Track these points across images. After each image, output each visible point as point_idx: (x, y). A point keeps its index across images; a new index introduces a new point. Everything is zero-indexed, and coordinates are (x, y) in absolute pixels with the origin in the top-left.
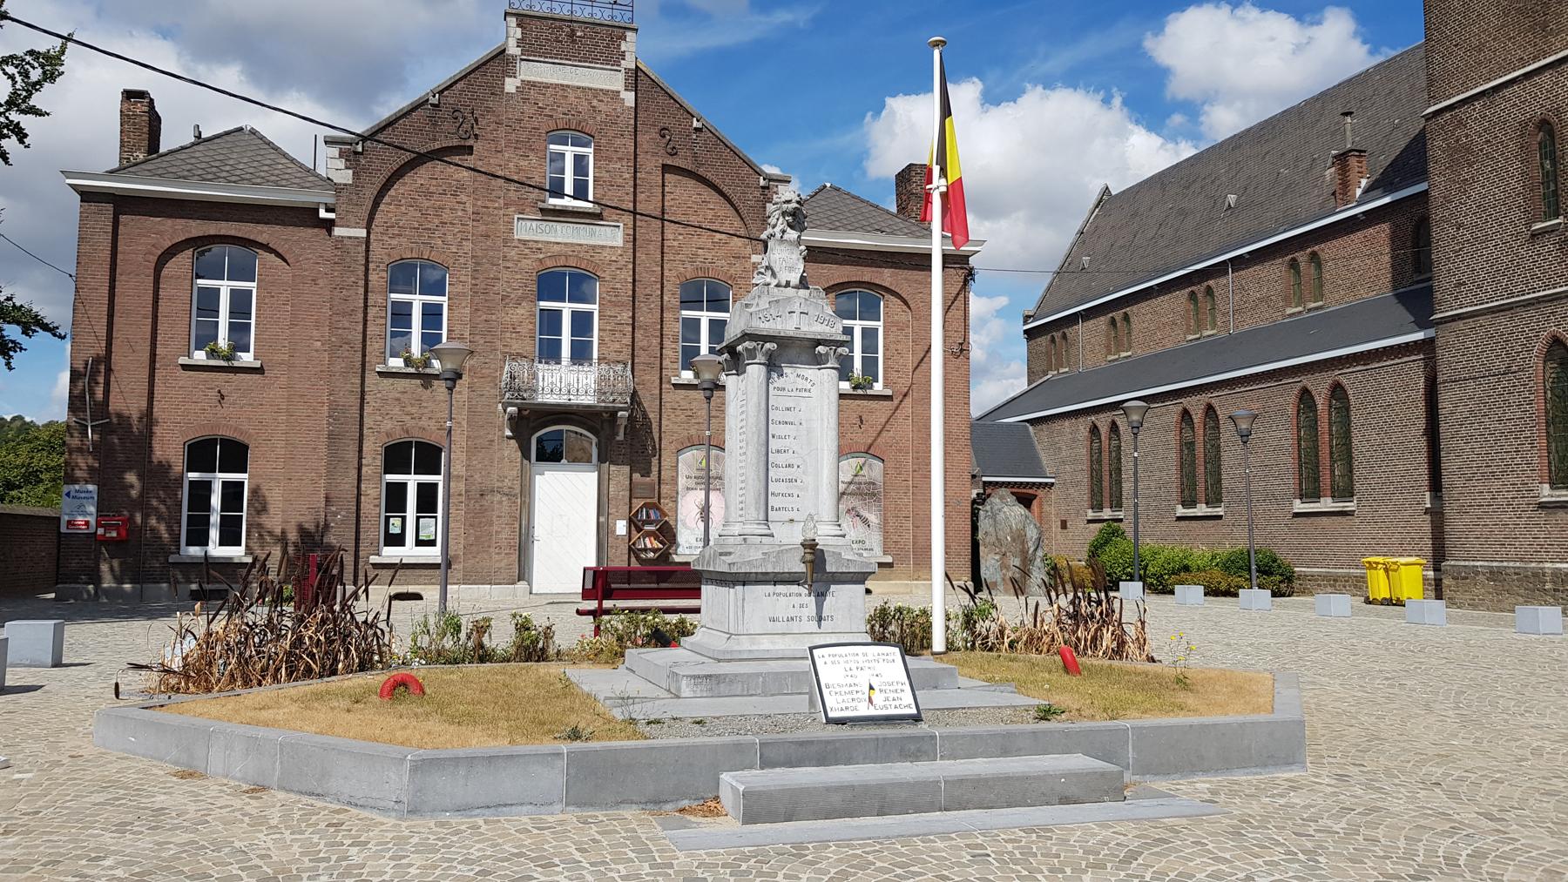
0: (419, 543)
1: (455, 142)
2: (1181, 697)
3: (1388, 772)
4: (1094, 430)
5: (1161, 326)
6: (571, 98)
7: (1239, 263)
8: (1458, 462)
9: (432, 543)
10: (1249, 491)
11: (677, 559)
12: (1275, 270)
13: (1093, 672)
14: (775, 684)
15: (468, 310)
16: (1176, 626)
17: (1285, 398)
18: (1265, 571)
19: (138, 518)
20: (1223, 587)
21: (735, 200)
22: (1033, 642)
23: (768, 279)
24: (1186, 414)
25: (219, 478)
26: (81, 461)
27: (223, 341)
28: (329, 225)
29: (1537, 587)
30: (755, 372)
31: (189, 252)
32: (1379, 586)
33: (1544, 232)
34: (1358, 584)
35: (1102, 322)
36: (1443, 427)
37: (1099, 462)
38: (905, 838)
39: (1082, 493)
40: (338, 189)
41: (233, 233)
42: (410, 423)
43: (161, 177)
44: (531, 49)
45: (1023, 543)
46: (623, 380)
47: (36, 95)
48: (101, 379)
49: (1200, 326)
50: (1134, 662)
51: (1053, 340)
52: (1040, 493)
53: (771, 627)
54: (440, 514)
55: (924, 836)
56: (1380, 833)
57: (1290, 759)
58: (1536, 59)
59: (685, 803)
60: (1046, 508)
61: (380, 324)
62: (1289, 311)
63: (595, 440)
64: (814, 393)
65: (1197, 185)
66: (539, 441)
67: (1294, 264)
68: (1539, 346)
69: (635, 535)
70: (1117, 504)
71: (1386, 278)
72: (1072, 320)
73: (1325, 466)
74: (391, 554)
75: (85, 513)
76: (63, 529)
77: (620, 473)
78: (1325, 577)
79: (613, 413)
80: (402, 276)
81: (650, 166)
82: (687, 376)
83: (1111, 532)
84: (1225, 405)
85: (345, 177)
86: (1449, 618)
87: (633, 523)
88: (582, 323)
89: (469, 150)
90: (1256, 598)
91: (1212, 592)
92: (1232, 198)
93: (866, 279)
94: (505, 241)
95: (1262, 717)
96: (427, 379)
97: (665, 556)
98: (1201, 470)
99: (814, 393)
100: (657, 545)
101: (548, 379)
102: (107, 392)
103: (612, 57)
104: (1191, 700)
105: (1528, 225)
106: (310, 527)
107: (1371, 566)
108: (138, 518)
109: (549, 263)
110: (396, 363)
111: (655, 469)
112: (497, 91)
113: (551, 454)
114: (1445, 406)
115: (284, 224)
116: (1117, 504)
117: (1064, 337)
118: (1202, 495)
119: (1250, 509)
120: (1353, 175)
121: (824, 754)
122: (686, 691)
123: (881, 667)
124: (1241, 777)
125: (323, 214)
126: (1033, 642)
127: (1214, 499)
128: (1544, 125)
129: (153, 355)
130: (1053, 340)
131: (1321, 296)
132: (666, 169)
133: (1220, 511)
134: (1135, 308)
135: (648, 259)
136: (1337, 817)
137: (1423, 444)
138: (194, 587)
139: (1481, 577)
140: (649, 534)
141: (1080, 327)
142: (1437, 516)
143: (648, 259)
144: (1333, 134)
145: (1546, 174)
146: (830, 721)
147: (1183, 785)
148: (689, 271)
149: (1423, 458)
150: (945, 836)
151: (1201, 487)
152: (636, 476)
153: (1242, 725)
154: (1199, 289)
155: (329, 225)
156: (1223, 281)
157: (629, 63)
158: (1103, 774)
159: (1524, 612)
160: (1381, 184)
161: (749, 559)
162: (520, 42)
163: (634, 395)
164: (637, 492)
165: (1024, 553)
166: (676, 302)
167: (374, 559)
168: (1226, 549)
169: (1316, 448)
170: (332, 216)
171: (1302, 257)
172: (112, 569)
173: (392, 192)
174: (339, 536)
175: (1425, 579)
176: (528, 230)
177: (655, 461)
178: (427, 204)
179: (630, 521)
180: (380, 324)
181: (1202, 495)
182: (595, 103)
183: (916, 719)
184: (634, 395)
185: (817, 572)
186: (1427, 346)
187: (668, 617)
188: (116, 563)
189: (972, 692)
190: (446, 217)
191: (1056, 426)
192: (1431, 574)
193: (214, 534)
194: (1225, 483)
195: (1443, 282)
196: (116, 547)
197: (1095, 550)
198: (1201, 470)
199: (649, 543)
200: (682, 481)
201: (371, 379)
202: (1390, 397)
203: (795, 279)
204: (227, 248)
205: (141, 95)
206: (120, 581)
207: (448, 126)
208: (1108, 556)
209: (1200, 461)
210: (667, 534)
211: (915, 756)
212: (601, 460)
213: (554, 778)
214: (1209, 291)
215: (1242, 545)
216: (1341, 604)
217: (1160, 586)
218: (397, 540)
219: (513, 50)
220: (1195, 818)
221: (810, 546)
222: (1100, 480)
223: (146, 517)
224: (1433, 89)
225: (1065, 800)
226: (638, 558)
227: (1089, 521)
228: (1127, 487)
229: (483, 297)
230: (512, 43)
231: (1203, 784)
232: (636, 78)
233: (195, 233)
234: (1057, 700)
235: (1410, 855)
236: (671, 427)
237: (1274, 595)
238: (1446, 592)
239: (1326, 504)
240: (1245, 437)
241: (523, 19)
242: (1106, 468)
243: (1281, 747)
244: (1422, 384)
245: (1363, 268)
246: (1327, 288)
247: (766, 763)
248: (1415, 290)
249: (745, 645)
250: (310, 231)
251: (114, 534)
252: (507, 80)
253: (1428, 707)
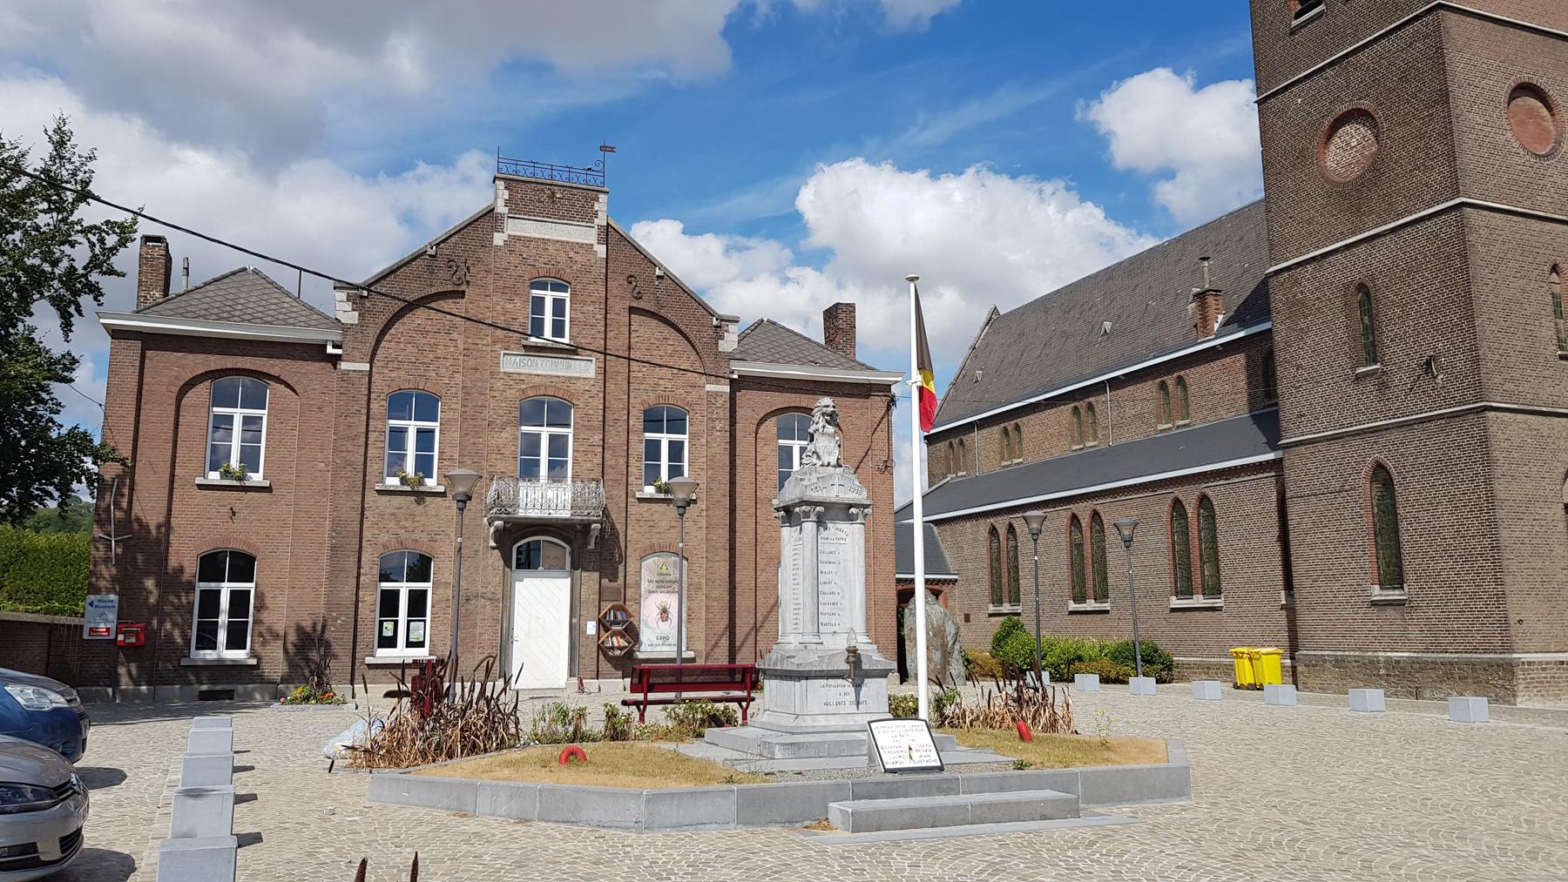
0: (410, 644)
1: (450, 288)
2: (1106, 754)
3: (1244, 801)
4: (993, 531)
5: (1049, 436)
6: (551, 248)
7: (1115, 383)
8: (1305, 566)
9: (421, 644)
10: (1132, 589)
11: (640, 656)
12: (1149, 388)
13: (1040, 741)
14: (836, 750)
15: (457, 435)
17: (1160, 506)
18: (1148, 661)
19: (155, 622)
21: (692, 337)
23: (814, 460)
24: (1074, 517)
25: (226, 589)
26: (103, 569)
27: (234, 463)
28: (335, 360)
29: (1368, 672)
30: (809, 526)
31: (207, 383)
32: (1246, 674)
33: (1366, 374)
34: (1227, 672)
35: (995, 431)
36: (1292, 536)
37: (998, 560)
39: (983, 589)
40: (345, 328)
41: (247, 366)
42: (404, 535)
43: (184, 316)
44: (517, 208)
45: (943, 637)
46: (595, 495)
47: (113, 259)
48: (126, 491)
50: (1062, 733)
52: (945, 588)
53: (825, 709)
54: (428, 618)
56: (1237, 831)
57: (1181, 793)
59: (807, 823)
61: (380, 448)
62: (1161, 427)
63: (568, 549)
64: (848, 539)
65: (1076, 311)
66: (519, 552)
67: (1163, 386)
68: (1366, 469)
69: (604, 636)
70: (1015, 599)
71: (1242, 401)
72: (969, 428)
73: (1198, 566)
74: (384, 655)
75: (106, 621)
76: (86, 636)
77: (591, 579)
78: (1200, 665)
79: (586, 526)
80: (399, 404)
81: (619, 307)
82: (650, 491)
83: (1012, 626)
84: (1111, 512)
85: (351, 317)
87: (602, 624)
88: (557, 445)
89: (462, 294)
90: (1143, 684)
91: (1105, 680)
92: (1107, 325)
93: (803, 405)
94: (492, 373)
96: (421, 496)
97: (630, 654)
99: (848, 539)
100: (623, 643)
101: (531, 496)
102: (130, 502)
103: (588, 216)
105: (1353, 368)
106: (307, 625)
107: (1238, 656)
108: (155, 622)
109: (530, 393)
110: (393, 482)
111: (621, 574)
112: (486, 243)
113: (528, 562)
115: (294, 358)
116: (1015, 599)
118: (1090, 592)
119: (1134, 606)
120: (1211, 311)
121: (891, 792)
122: (778, 755)
123: (915, 735)
124: (1150, 805)
125: (330, 350)
126: (988, 721)
127: (1102, 595)
128: (1362, 287)
129: (172, 476)
131: (1188, 415)
132: (632, 310)
133: (1107, 606)
134: (1025, 419)
135: (616, 388)
137: (1277, 549)
138: (204, 687)
139: (1328, 665)
140: (615, 634)
141: (976, 435)
142: (1290, 610)
143: (616, 388)
144: (1194, 272)
145: (1365, 328)
146: (887, 771)
148: (651, 399)
149: (1278, 561)
151: (1089, 584)
152: (605, 581)
153: (1149, 770)
154: (1082, 405)
155: (335, 360)
157: (601, 220)
158: (1066, 801)
159: (1354, 693)
160: (1233, 321)
161: (810, 661)
162: (507, 203)
163: (605, 510)
164: (606, 595)
166: (640, 425)
167: (369, 660)
169: (1188, 551)
170: (339, 351)
171: (1170, 380)
172: (129, 673)
173: (392, 331)
174: (338, 637)
175: (1283, 666)
176: (513, 364)
177: (621, 568)
178: (423, 341)
179: (600, 622)
180: (380, 448)
181: (1090, 592)
182: (572, 254)
183: (941, 769)
184: (605, 510)
185: (856, 671)
186: (1277, 465)
187: (717, 705)
188: (134, 668)
190: (439, 353)
191: (958, 527)
193: (222, 636)
194: (1110, 581)
195: (1287, 414)
196: (133, 652)
197: (999, 641)
198: (1089, 569)
199: (617, 641)
200: (644, 585)
201: (370, 496)
203: (834, 462)
204: (241, 379)
205: (159, 239)
206: (137, 683)
207: (444, 274)
208: (1012, 645)
209: (1088, 561)
210: (632, 633)
211: (947, 792)
212: (574, 567)
213: (729, 807)
214: (1090, 407)
215: (1127, 637)
216: (1213, 689)
218: (390, 642)
219: (501, 209)
220: (1126, 825)
221: (853, 651)
222: (1000, 577)
223: (161, 623)
226: (605, 655)
229: (472, 423)
230: (500, 203)
231: (1126, 809)
232: (607, 233)
233: (213, 368)
234: (1025, 757)
236: (634, 537)
238: (1301, 678)
239: (1198, 601)
240: (1128, 542)
241: (510, 183)
242: (1004, 567)
243: (1174, 785)
244: (1274, 497)
245: (1222, 392)
246: (1192, 407)
247: (856, 797)
248: (1266, 417)
249: (809, 722)
250: (317, 364)
251: (133, 640)
252: (496, 235)
253: (1274, 763)
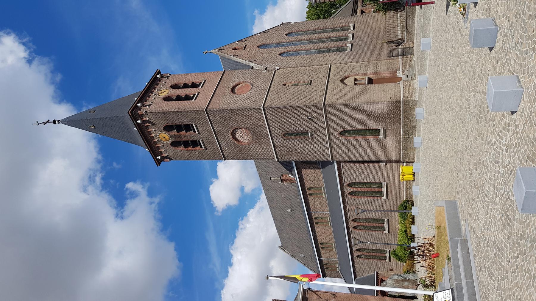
2: (442, 227)
3: (456, 183)
4: (359, 256)
7: (308, 209)
10: (380, 211)
12: (311, 199)
13: (438, 250)
16: (423, 231)
17: (351, 199)
18: (406, 208)
20: (411, 220)
22: (431, 268)
24: (354, 227)
32: (410, 177)
33: (311, 135)
34: (408, 183)
35: (322, 252)
36: (362, 160)
37: (369, 256)
38: (479, 287)
39: (380, 262)
45: (399, 280)
49: (327, 222)
50: (435, 241)
51: (327, 268)
52: (380, 277)
55: (478, 283)
58: (268, 136)
60: (385, 275)
62: (324, 196)
67: (310, 195)
71: (317, 171)
73: (373, 190)
78: (407, 191)
83: (394, 253)
84: (353, 215)
86: (419, 136)
90: (414, 211)
91: (413, 223)
95: (445, 209)
98: (373, 225)
104: (443, 225)
105: (309, 139)
107: (403, 179)
114: (356, 159)
116: (384, 251)
117: (326, 264)
118: (381, 225)
119: (386, 211)
120: (287, 178)
123: (440, 298)
124: (460, 214)
127: (382, 221)
128: (284, 135)
130: (327, 268)
131: (321, 188)
133: (386, 220)
136: (466, 195)
137: (366, 165)
141: (323, 259)
144: (274, 182)
145: (297, 135)
147: (463, 227)
149: (370, 165)
150: (478, 278)
151: (378, 225)
153: (447, 213)
156: (313, 214)
160: (291, 171)
165: (403, 280)
168: (398, 219)
171: (308, 192)
175: (406, 166)
181: (381, 225)
183: (452, 290)
186: (338, 163)
189: (445, 281)
191: (357, 269)
192: (405, 164)
194: (377, 218)
195: (322, 158)
197: (400, 259)
198: (373, 225)
202: (352, 172)
209: (370, 224)
214: (316, 218)
215: (397, 214)
216: (415, 188)
217: (412, 238)
224: (271, 159)
225: (468, 253)
227: (390, 261)
228: (378, 247)
231: (462, 223)
235: (470, 182)
237: (413, 206)
239: (384, 190)
240: (363, 211)
242: (372, 254)
243: (452, 206)
244: (349, 164)
245: (313, 177)
246: (318, 186)
